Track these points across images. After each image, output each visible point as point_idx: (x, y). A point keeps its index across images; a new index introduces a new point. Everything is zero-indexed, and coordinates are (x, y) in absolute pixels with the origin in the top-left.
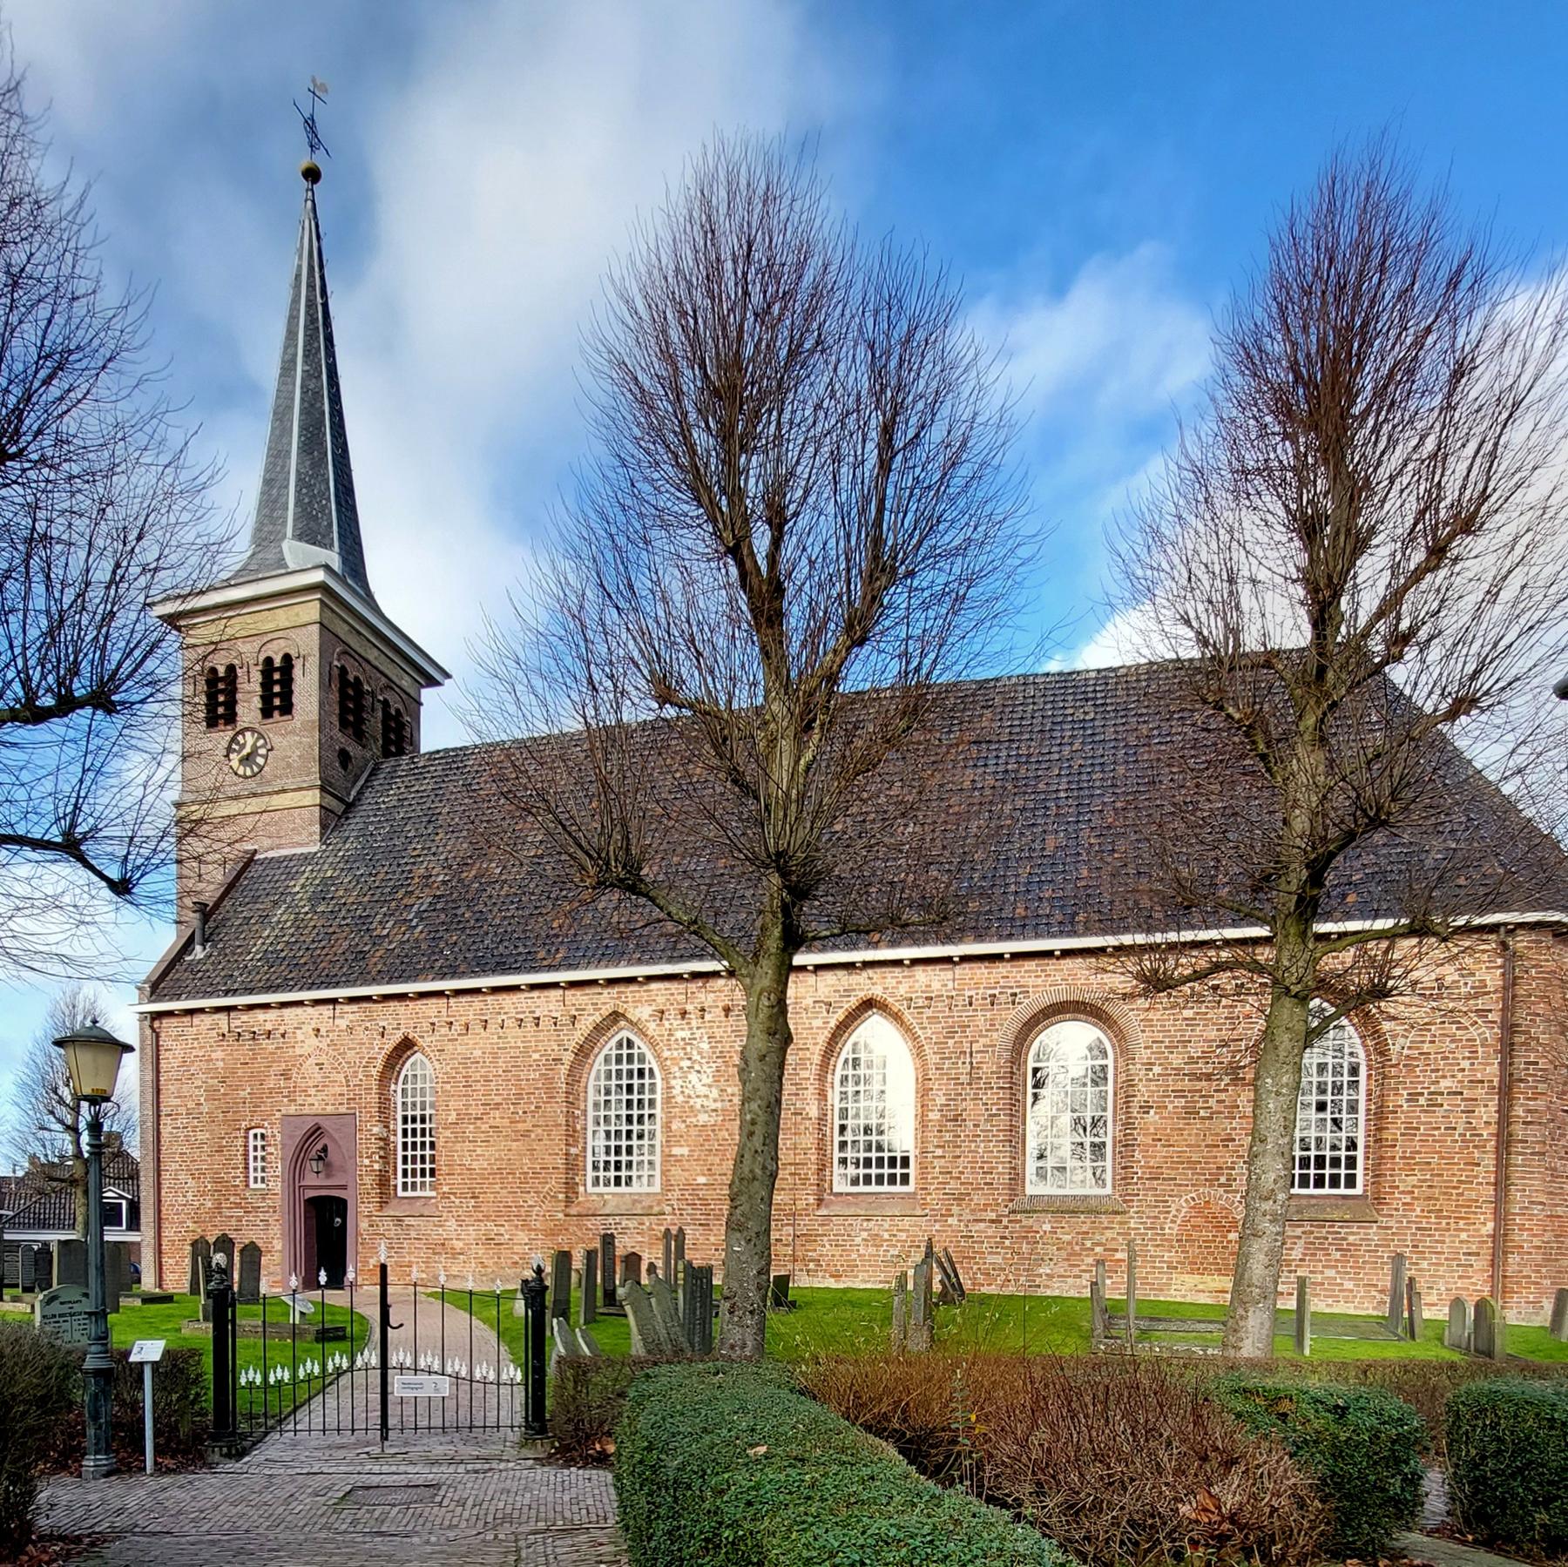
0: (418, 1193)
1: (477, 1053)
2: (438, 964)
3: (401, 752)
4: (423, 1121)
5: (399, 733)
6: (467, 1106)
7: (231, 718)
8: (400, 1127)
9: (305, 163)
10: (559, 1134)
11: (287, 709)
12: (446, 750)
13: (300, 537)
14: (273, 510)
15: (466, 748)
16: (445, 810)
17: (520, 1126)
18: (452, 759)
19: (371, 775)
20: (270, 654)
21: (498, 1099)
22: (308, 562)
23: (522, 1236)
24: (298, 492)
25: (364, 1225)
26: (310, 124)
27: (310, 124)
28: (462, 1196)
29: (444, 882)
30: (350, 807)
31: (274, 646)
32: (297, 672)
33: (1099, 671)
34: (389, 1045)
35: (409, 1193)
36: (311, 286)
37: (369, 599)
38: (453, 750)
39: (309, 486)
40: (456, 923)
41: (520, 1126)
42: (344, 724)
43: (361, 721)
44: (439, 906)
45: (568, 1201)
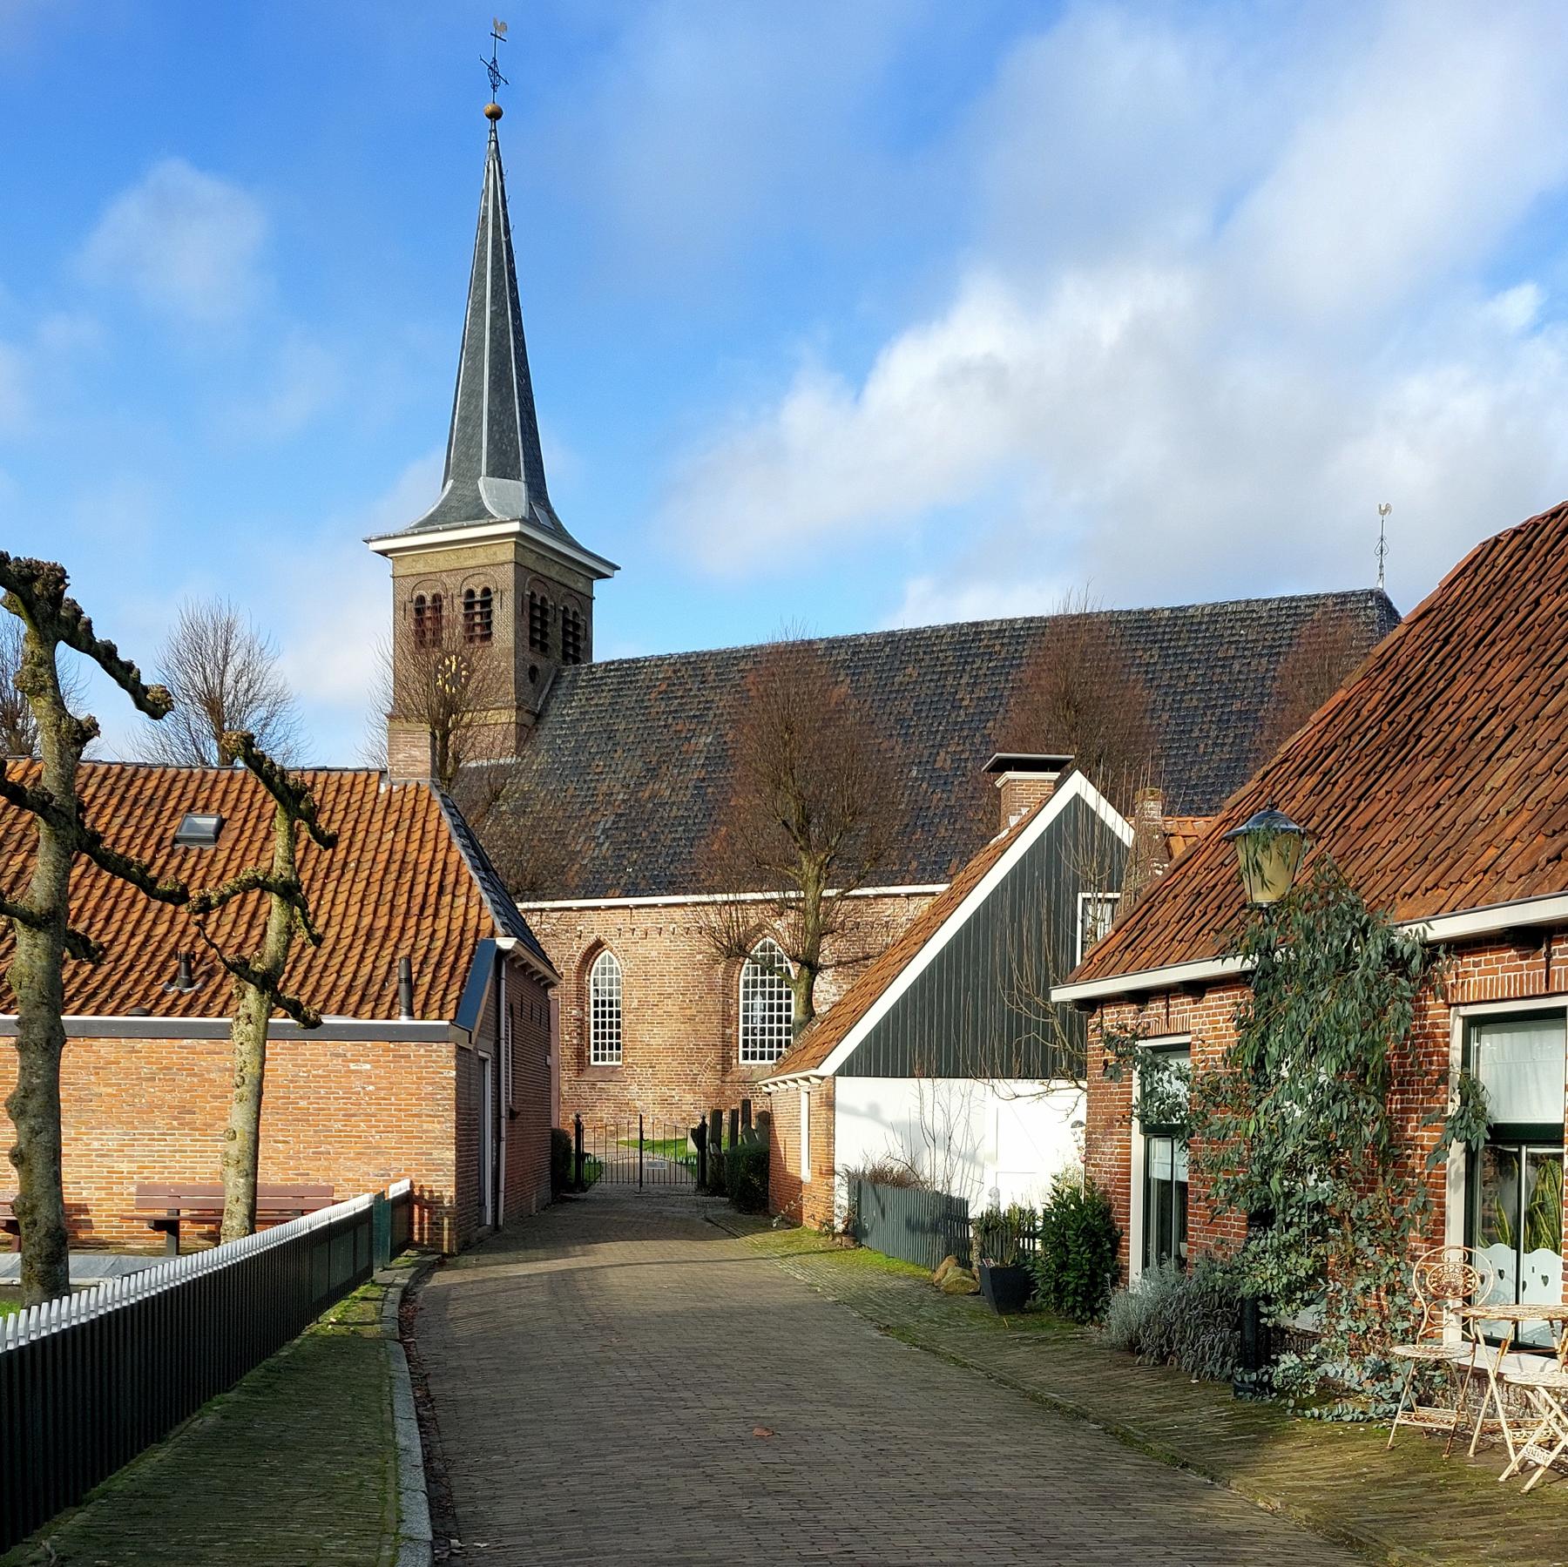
0: (607, 1063)
1: (654, 954)
2: (623, 882)
3: (577, 660)
4: (611, 1005)
6: (646, 995)
8: (592, 1009)
9: (489, 108)
10: (716, 1019)
11: (487, 637)
12: (621, 662)
13: (492, 473)
14: (469, 448)
15: (638, 660)
16: (622, 727)
17: (688, 1012)
18: (627, 670)
19: (554, 683)
20: (472, 587)
21: (670, 990)
22: (503, 498)
23: (689, 1098)
24: (490, 429)
25: (565, 1088)
26: (493, 70)
27: (493, 70)
28: (642, 1066)
29: (624, 801)
30: (538, 717)
31: (476, 579)
32: (495, 605)
33: (1172, 610)
34: (585, 945)
35: (600, 1063)
36: (496, 227)
38: (626, 661)
39: (499, 423)
40: (634, 843)
41: (688, 1012)
42: (533, 642)
43: (545, 635)
44: (621, 825)
45: (725, 1071)
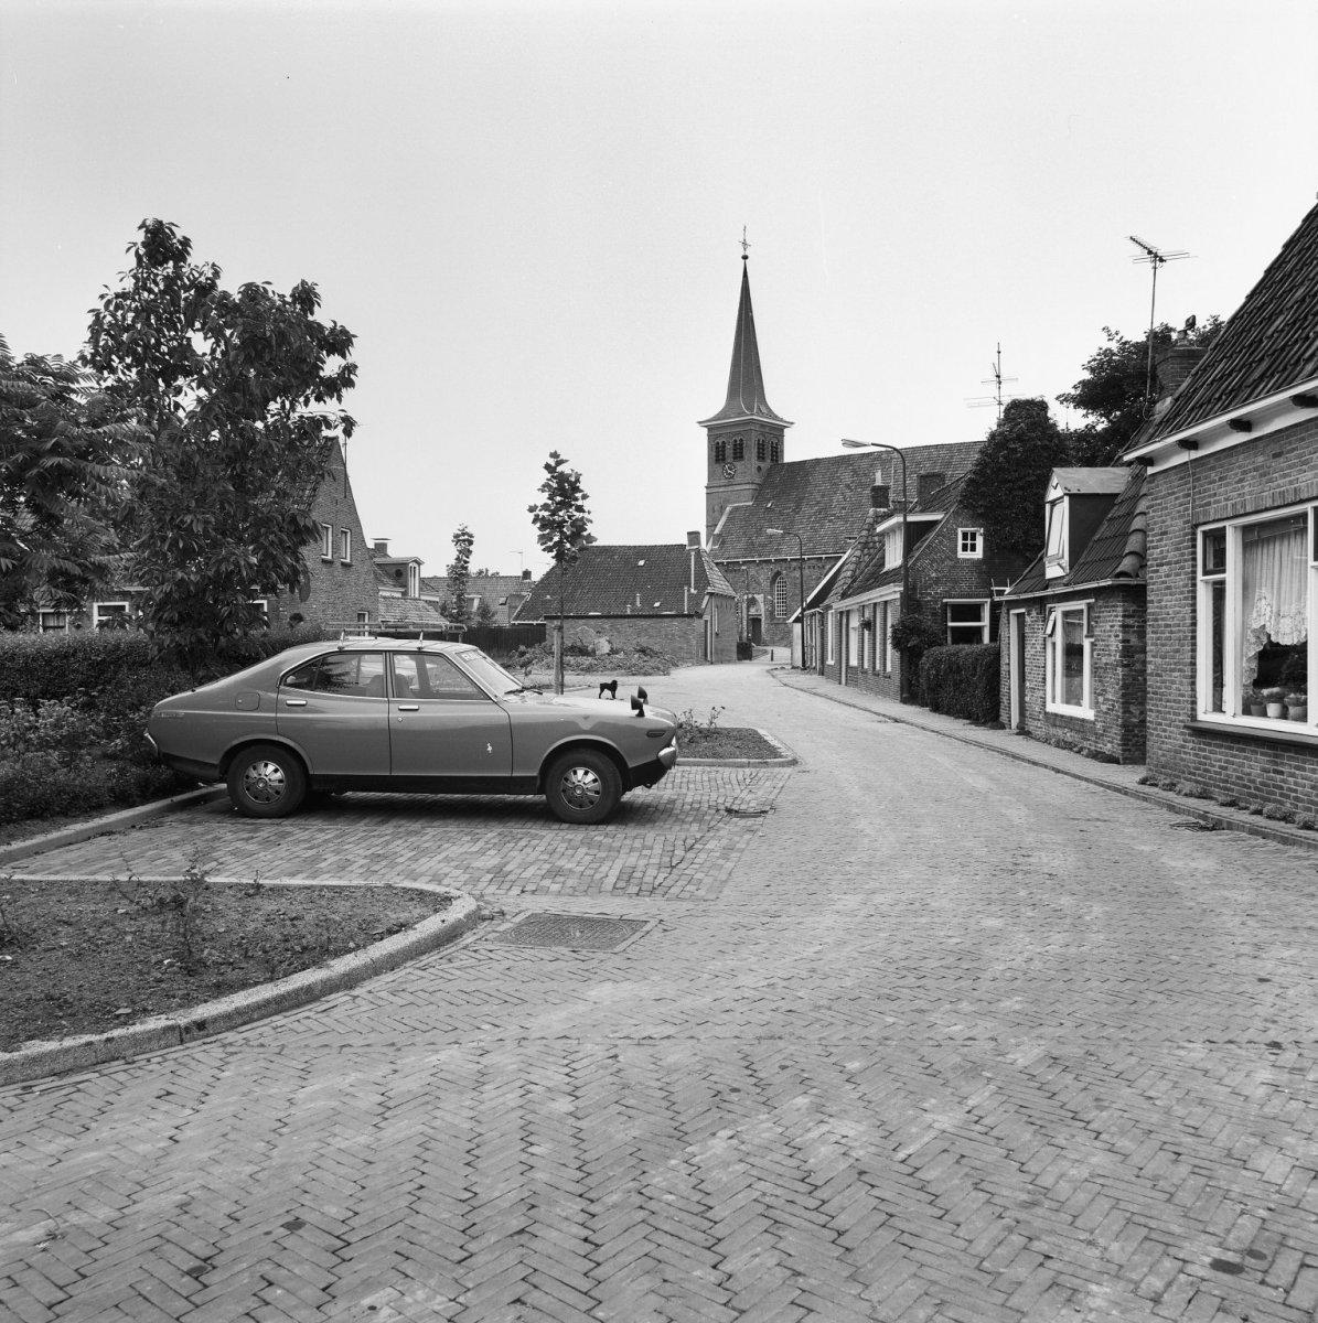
5: (777, 451)
7: (724, 459)
37: (776, 417)
